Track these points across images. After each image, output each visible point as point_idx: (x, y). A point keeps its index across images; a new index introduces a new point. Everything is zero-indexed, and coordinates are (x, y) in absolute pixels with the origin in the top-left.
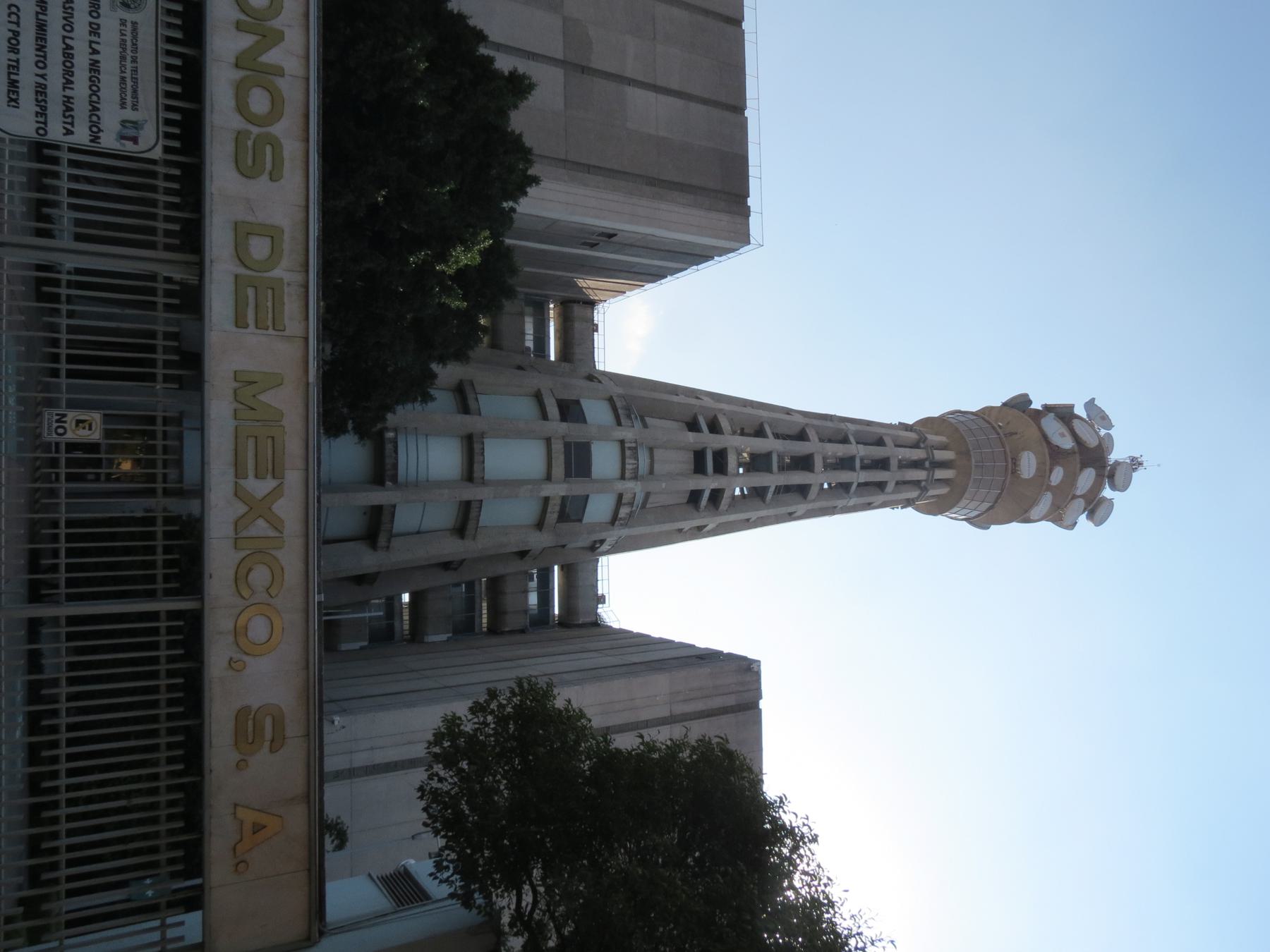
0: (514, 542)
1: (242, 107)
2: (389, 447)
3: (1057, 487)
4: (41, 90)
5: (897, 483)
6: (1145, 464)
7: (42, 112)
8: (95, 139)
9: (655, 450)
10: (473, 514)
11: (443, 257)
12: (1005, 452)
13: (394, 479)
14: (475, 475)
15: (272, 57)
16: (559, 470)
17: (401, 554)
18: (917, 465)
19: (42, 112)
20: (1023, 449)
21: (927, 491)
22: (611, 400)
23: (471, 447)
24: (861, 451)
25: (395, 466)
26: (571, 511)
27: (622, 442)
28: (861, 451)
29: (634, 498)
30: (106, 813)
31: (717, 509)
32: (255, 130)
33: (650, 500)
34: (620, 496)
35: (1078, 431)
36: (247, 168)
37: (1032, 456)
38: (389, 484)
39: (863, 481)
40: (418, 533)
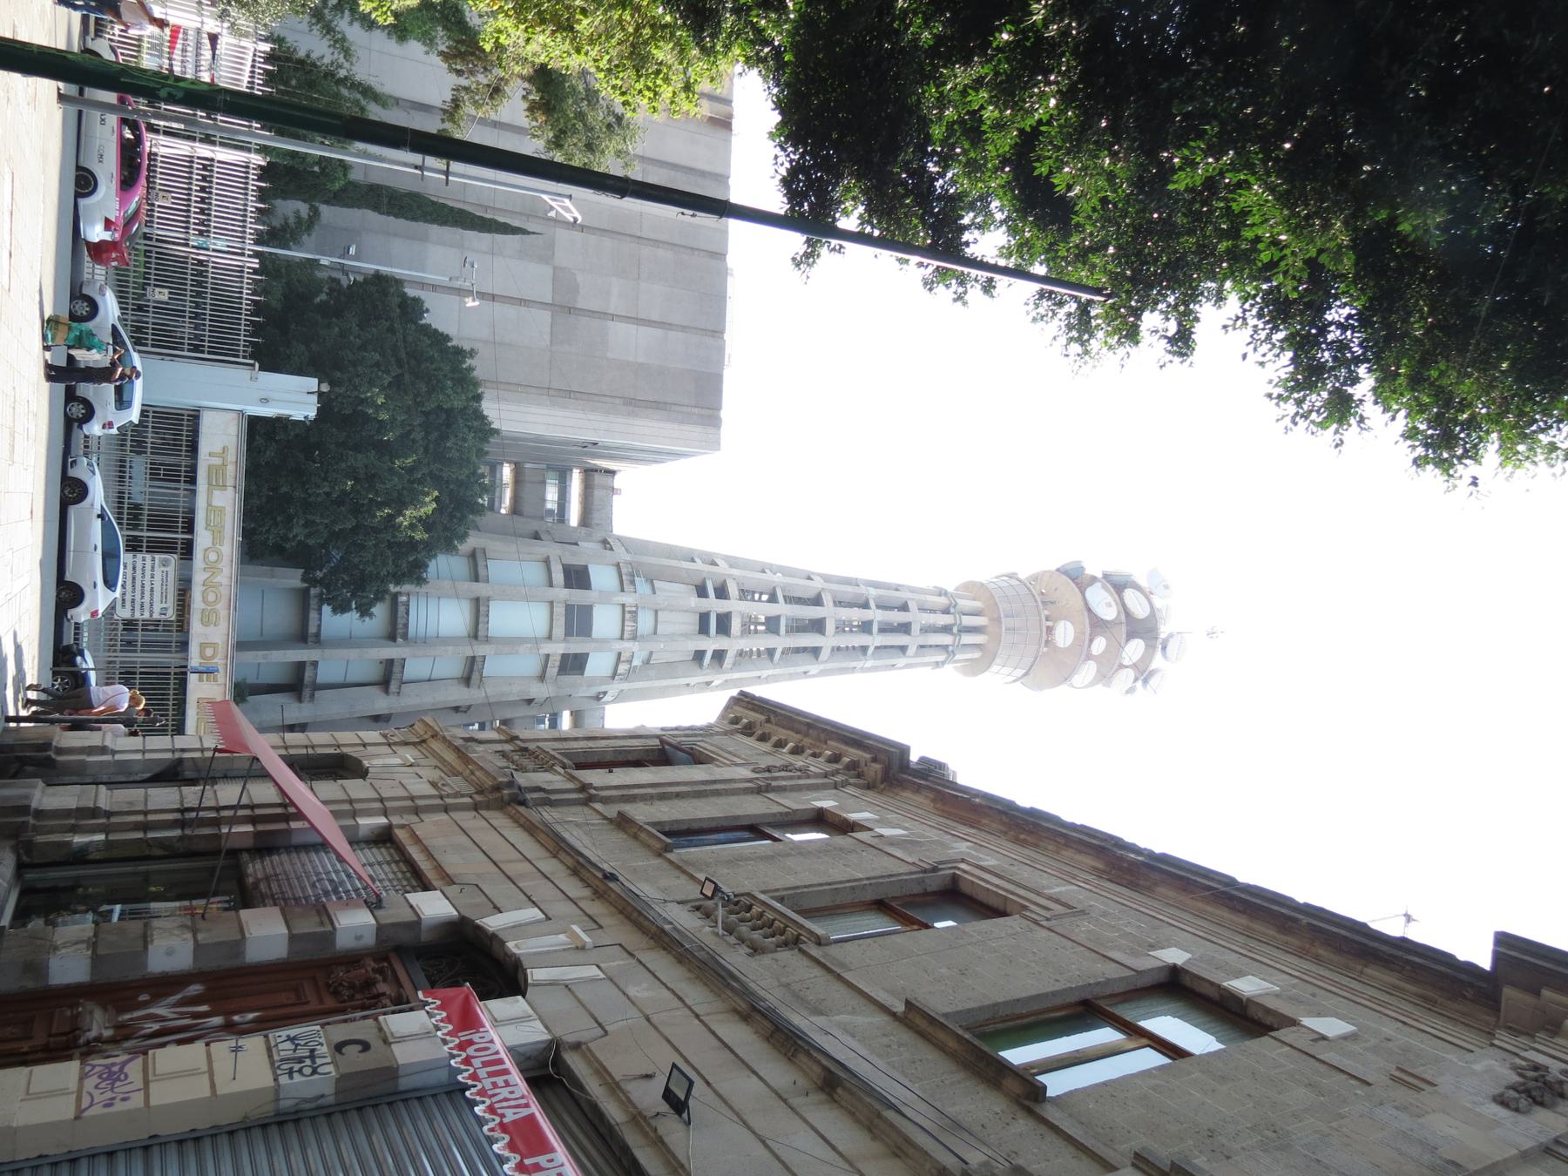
0: (515, 692)
1: (205, 600)
2: (401, 609)
3: (1101, 656)
4: (133, 601)
7: (133, 609)
8: (151, 616)
9: (659, 613)
11: (400, 513)
13: (405, 636)
14: (480, 633)
15: (218, 579)
16: (559, 630)
18: (946, 629)
19: (133, 609)
20: (1065, 618)
21: (954, 655)
22: (618, 566)
23: (479, 608)
25: (406, 626)
26: (573, 664)
27: (623, 606)
28: (876, 616)
29: (633, 657)
30: (226, 196)
31: (721, 667)
32: (209, 608)
33: (654, 657)
34: (620, 654)
35: (1127, 601)
36: (206, 622)
37: (1069, 626)
38: (399, 640)
39: (879, 645)
40: (429, 680)
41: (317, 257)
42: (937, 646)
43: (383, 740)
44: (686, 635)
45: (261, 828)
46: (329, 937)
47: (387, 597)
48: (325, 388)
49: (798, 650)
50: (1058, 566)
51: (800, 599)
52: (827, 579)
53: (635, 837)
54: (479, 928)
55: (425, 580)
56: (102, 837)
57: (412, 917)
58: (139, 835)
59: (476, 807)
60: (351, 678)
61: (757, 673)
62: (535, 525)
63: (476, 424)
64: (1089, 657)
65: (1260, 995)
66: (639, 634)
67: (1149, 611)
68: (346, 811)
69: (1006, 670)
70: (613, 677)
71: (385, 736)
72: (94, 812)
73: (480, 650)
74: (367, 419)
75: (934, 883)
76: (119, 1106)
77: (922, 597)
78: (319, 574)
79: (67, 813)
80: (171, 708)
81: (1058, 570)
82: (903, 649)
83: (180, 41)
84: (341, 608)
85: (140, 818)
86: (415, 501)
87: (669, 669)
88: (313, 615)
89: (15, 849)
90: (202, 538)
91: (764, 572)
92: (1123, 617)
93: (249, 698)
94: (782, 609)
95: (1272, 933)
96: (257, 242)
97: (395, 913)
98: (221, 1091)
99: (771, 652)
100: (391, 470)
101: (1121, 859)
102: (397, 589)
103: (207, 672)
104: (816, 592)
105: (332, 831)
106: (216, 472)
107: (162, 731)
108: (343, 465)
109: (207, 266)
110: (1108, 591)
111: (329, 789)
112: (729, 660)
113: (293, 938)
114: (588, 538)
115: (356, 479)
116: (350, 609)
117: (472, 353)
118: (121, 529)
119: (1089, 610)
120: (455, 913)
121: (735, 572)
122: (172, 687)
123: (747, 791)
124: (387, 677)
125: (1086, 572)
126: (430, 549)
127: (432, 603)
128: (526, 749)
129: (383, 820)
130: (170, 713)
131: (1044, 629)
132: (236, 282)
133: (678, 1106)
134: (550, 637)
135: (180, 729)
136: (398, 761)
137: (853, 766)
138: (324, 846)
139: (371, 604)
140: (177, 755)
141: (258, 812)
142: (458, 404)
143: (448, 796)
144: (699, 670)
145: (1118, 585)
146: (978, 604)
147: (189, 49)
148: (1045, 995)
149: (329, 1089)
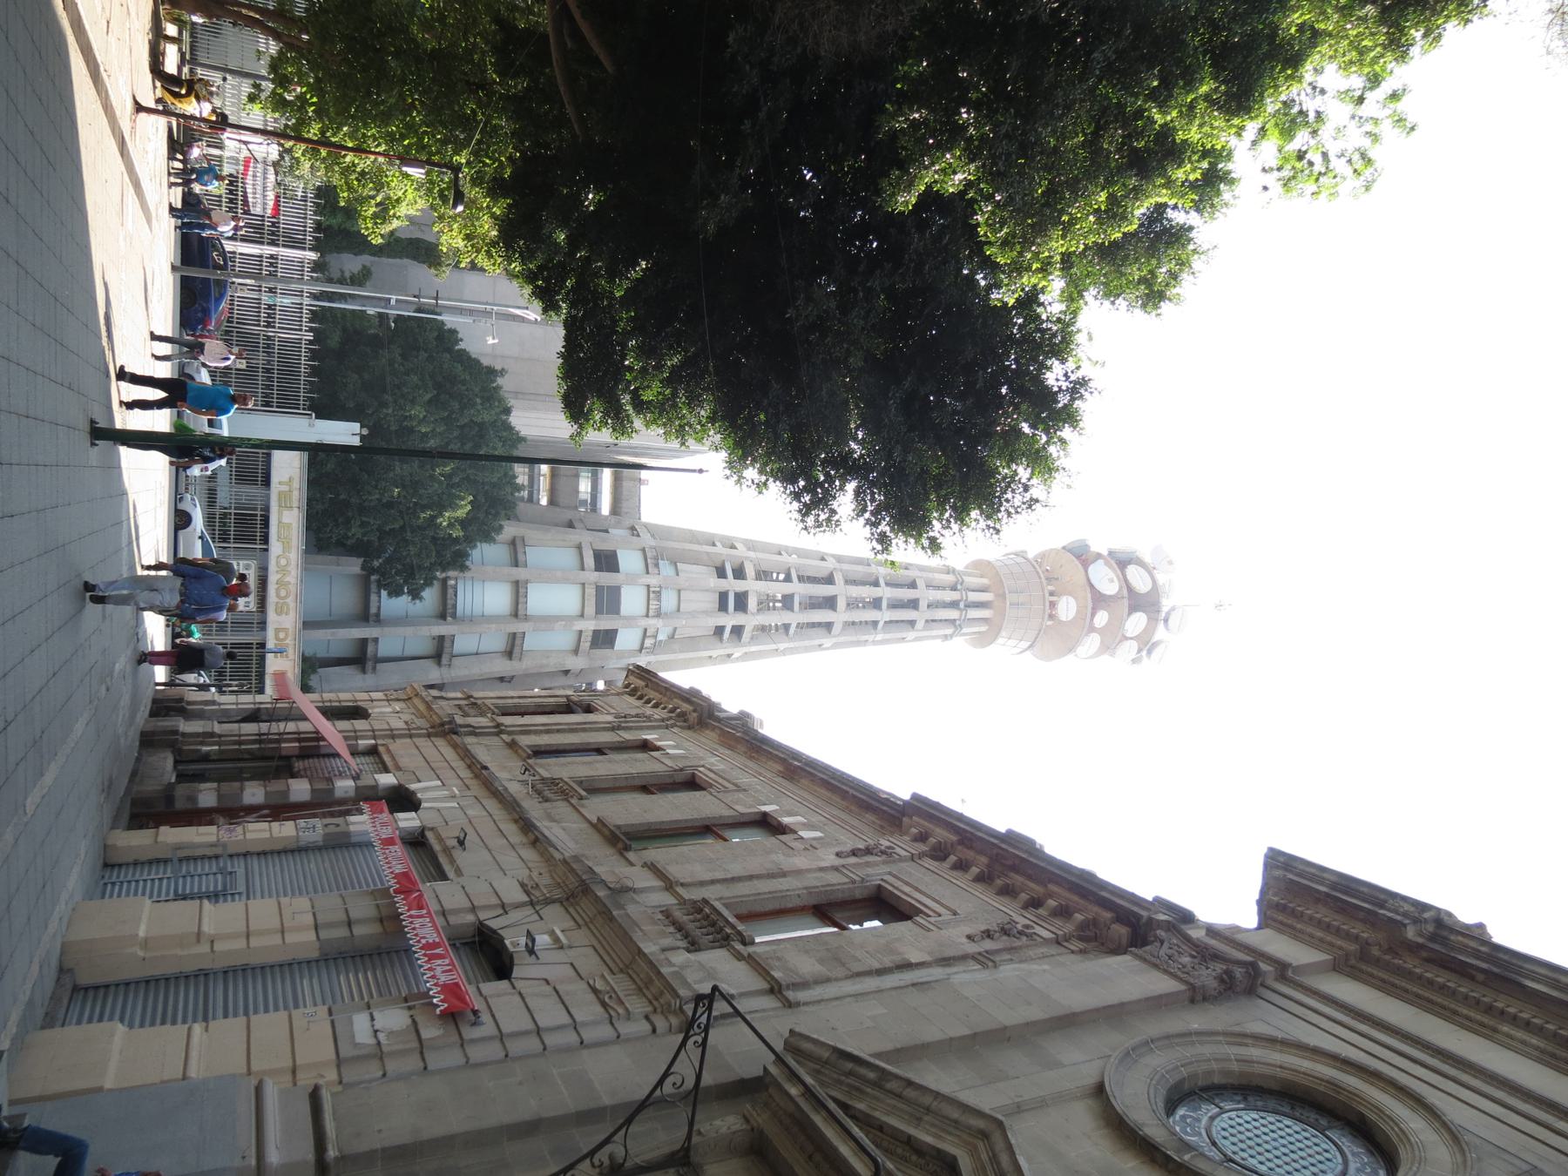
0: (553, 664)
1: (278, 596)
2: (450, 591)
5: (927, 621)
9: (682, 592)
10: (518, 642)
13: (454, 616)
14: (520, 613)
15: (287, 579)
16: (590, 609)
17: (460, 670)
18: (954, 605)
20: (1070, 594)
21: (961, 628)
22: (643, 550)
24: (886, 593)
25: (455, 606)
27: (648, 586)
28: (886, 593)
37: (1072, 601)
38: (449, 619)
39: (888, 619)
40: (477, 654)
41: (364, 308)
42: (946, 620)
43: (384, 698)
44: (706, 613)
45: (303, 744)
46: (331, 791)
47: (435, 582)
48: (365, 432)
49: (813, 625)
50: (1064, 544)
51: (809, 577)
52: (839, 559)
53: (516, 752)
54: (407, 789)
55: (467, 567)
56: (217, 747)
57: (374, 784)
58: (237, 747)
59: (429, 735)
60: (408, 653)
61: (774, 646)
62: (568, 515)
63: (505, 434)
64: (1092, 629)
66: (663, 611)
67: (1117, 589)
68: (348, 737)
69: (1012, 642)
70: (640, 651)
71: (386, 695)
72: (212, 735)
73: (518, 627)
74: (411, 430)
75: (680, 778)
76: (233, 839)
78: (376, 563)
79: (197, 735)
80: (254, 678)
81: (1064, 548)
82: (912, 623)
83: (251, 169)
84: (395, 592)
85: (237, 738)
86: (454, 507)
87: (692, 642)
88: (373, 597)
89: (173, 752)
91: (780, 554)
92: (1125, 592)
93: (319, 670)
94: (796, 588)
95: (838, 800)
96: (311, 321)
97: (366, 781)
98: (274, 835)
99: (786, 627)
100: (432, 477)
101: (791, 764)
102: (444, 575)
103: (279, 652)
104: (829, 572)
105: (340, 746)
106: (284, 498)
107: (248, 692)
108: (391, 475)
109: (277, 259)
110: (1110, 567)
111: (344, 725)
112: (746, 635)
113: (313, 791)
114: (618, 525)
115: (404, 487)
116: (403, 593)
117: (503, 372)
118: (213, 542)
119: (1092, 586)
120: (396, 782)
121: (752, 554)
122: (254, 662)
123: (605, 729)
124: (439, 651)
125: (1092, 549)
126: (470, 541)
127: (478, 587)
128: (475, 704)
129: (373, 742)
130: (254, 682)
131: (1047, 604)
132: (296, 330)
133: (461, 843)
134: (582, 615)
135: (261, 691)
136: (389, 710)
137: (683, 715)
138: (337, 755)
139: (422, 588)
140: (257, 706)
141: (302, 736)
142: (486, 417)
143: (414, 729)
144: (785, 637)
145: (1122, 562)
146: (985, 581)
147: (258, 174)
148: (680, 821)
149: (320, 839)
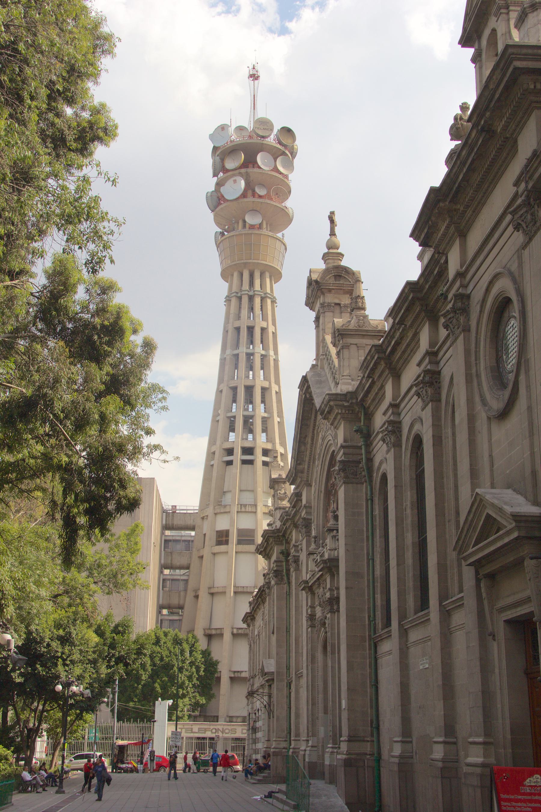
2: (240, 631)
6: (254, 63)
12: (245, 234)
21: (267, 293)
65: (481, 81)
77: (232, 316)
90: (208, 734)
146: (236, 274)
